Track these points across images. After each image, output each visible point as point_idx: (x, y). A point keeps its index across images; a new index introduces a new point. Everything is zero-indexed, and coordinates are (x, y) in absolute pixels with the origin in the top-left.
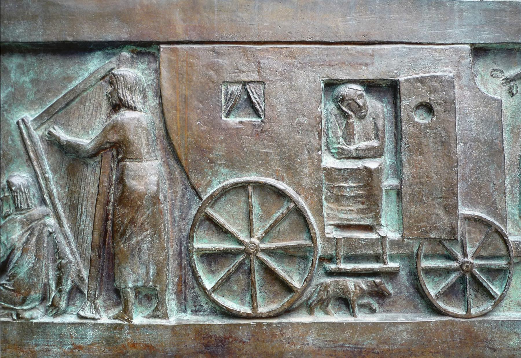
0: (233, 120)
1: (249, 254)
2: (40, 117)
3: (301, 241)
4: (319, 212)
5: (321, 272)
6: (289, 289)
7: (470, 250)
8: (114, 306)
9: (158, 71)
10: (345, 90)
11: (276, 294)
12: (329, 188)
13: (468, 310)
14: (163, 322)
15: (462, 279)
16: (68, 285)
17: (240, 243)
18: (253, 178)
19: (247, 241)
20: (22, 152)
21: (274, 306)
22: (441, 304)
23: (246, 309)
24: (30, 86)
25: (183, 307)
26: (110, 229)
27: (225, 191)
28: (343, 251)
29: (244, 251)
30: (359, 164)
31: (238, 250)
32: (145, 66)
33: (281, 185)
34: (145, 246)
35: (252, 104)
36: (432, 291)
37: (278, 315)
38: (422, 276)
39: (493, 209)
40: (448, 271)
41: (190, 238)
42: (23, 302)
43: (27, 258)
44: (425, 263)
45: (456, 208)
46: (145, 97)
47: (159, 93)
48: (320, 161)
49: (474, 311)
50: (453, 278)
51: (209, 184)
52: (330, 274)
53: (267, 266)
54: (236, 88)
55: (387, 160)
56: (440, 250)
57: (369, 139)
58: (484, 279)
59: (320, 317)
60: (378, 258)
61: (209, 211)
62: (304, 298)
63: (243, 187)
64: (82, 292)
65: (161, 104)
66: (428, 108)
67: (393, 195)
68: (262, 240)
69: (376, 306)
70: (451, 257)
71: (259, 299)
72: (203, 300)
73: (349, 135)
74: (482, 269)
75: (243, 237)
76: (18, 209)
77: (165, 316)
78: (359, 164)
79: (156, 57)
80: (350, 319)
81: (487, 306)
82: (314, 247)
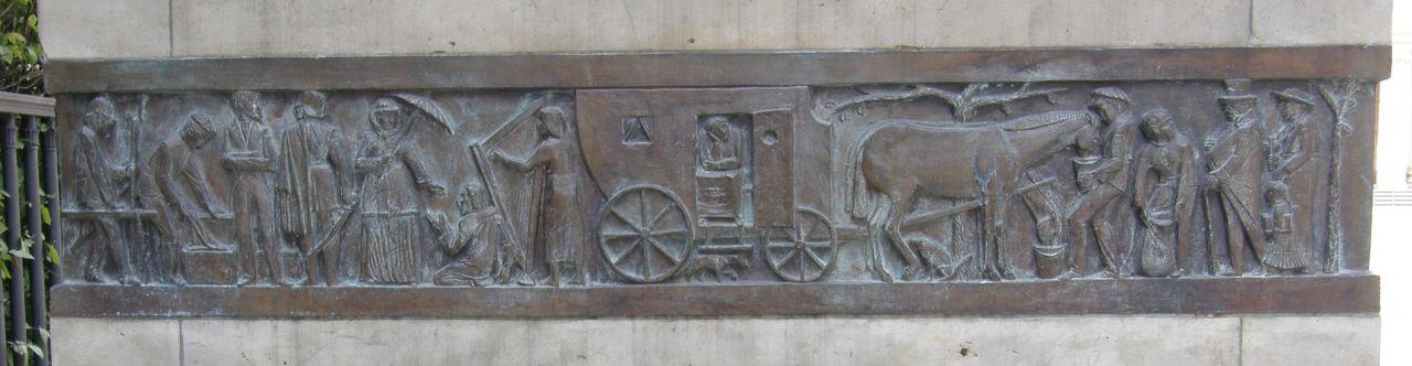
0: (631, 144)
1: (642, 239)
2: (488, 142)
3: (681, 229)
4: (693, 209)
5: (696, 251)
6: (671, 262)
7: (803, 234)
8: (544, 277)
9: (574, 108)
10: (712, 121)
11: (663, 267)
12: (702, 192)
13: (802, 277)
14: (581, 287)
15: (797, 255)
16: (511, 262)
17: (636, 230)
18: (647, 185)
19: (641, 229)
20: (474, 167)
21: (661, 275)
22: (783, 273)
23: (641, 277)
24: (477, 118)
25: (594, 277)
26: (541, 222)
27: (624, 196)
28: (711, 236)
29: (639, 236)
30: (722, 174)
31: (665, 244)
32: (564, 104)
33: (666, 190)
34: (568, 234)
35: (645, 133)
36: (776, 263)
37: (664, 281)
38: (768, 253)
39: (820, 205)
40: (789, 249)
41: (599, 228)
42: (480, 274)
43: (482, 243)
44: (772, 244)
45: (792, 203)
46: (565, 128)
47: (575, 124)
48: (694, 172)
49: (806, 278)
50: (790, 255)
51: (613, 190)
52: (702, 252)
53: (1358, 312)
54: (633, 120)
55: (746, 170)
56: (781, 235)
57: (730, 156)
58: (814, 256)
59: (694, 282)
60: (737, 241)
61: (613, 208)
62: (683, 269)
63: (638, 191)
64: (521, 268)
65: (577, 133)
66: (772, 133)
67: (749, 195)
68: (652, 229)
69: (735, 275)
70: (789, 239)
71: (651, 270)
72: (610, 272)
73: (715, 154)
74: (813, 249)
75: (638, 226)
76: (474, 208)
77: (583, 283)
78: (722, 174)
79: (573, 97)
80: (718, 284)
81: (817, 274)
82: (690, 234)
